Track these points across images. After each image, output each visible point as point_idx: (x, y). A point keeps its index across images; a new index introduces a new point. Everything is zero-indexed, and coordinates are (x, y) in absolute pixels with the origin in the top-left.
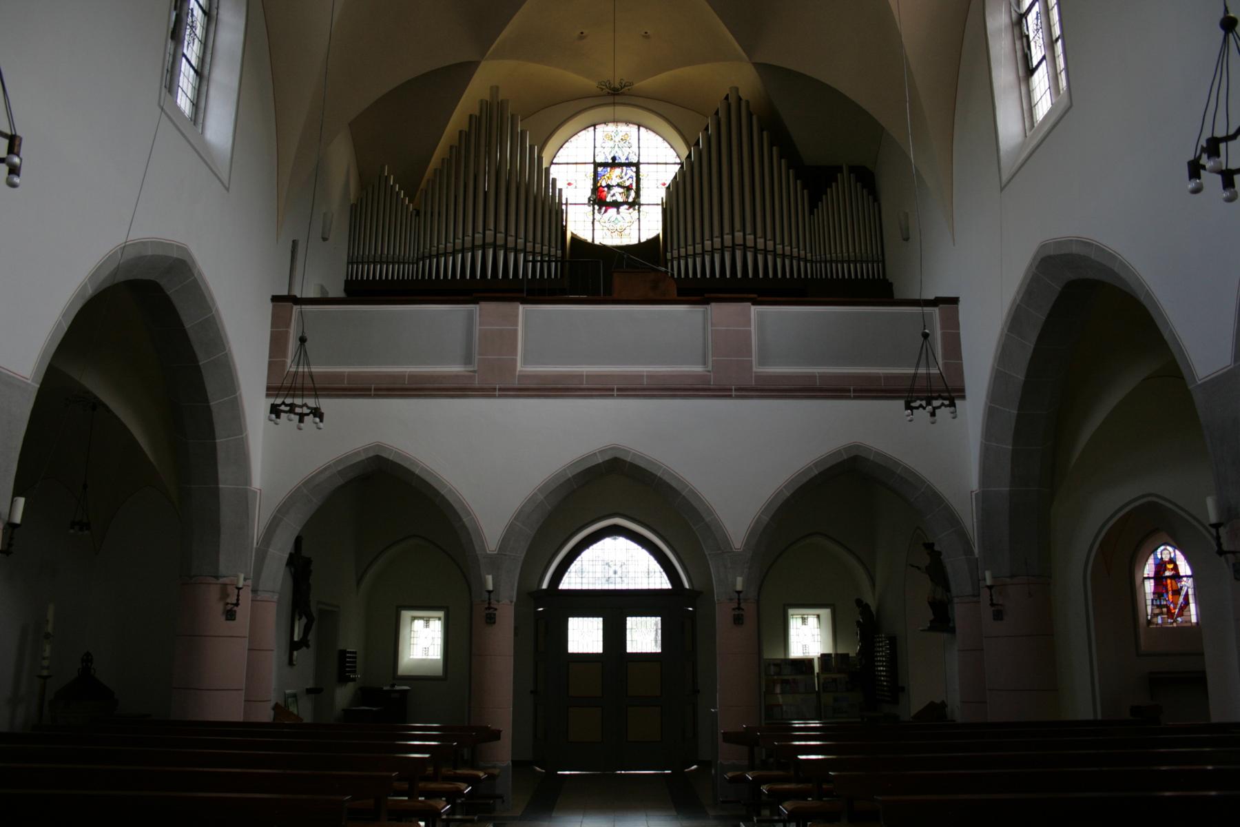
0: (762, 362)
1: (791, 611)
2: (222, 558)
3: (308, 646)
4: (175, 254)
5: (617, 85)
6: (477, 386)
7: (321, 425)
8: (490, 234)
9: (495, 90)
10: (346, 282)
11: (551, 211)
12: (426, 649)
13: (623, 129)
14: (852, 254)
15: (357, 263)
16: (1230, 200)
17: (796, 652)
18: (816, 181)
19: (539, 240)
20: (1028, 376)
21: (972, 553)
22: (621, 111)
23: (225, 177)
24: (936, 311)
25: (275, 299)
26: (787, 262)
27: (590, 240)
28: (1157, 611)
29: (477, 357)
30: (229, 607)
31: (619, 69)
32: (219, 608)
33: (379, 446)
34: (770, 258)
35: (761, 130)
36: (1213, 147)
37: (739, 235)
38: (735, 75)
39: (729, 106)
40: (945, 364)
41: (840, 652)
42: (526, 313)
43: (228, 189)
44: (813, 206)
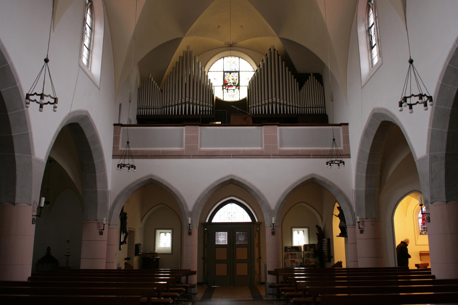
0: (281, 145)
1: (293, 229)
2: (98, 214)
3: (126, 243)
4: (84, 114)
5: (231, 43)
6: (185, 154)
7: (135, 170)
8: (187, 99)
9: (188, 47)
10: (137, 116)
11: (208, 90)
12: (165, 244)
13: (233, 58)
14: (314, 105)
15: (141, 109)
16: (411, 113)
17: (295, 244)
18: (301, 79)
19: (204, 101)
20: (370, 151)
21: (353, 211)
22: (232, 52)
23: (98, 85)
24: (341, 128)
25: (115, 125)
26: (291, 108)
27: (222, 99)
28: (423, 230)
29: (184, 145)
30: (101, 231)
31: (232, 39)
32: (97, 231)
33: (151, 175)
34: (285, 107)
35: (282, 61)
36: (405, 99)
37: (274, 99)
38: (273, 41)
39: (271, 52)
40: (344, 146)
41: (311, 243)
42: (201, 129)
43: (99, 89)
44: (300, 88)
